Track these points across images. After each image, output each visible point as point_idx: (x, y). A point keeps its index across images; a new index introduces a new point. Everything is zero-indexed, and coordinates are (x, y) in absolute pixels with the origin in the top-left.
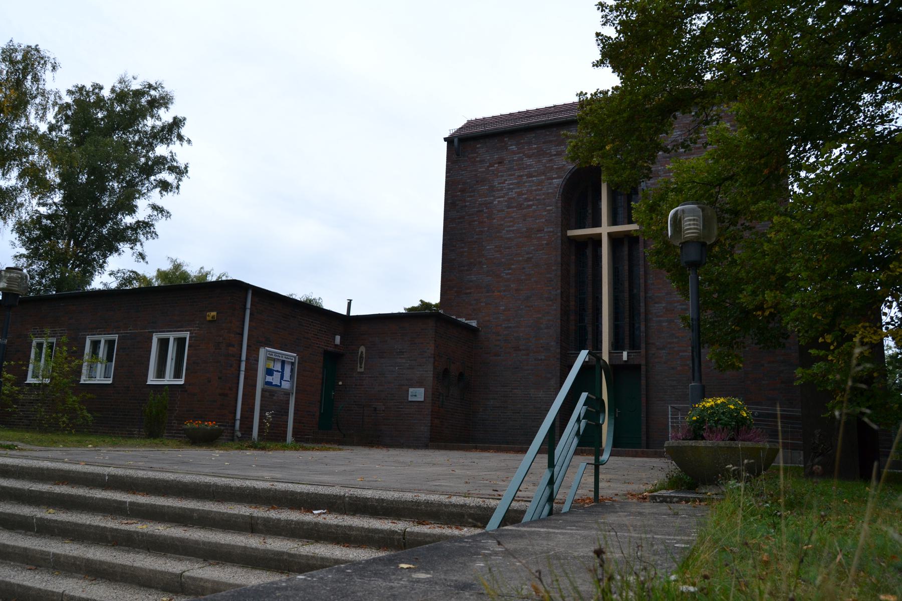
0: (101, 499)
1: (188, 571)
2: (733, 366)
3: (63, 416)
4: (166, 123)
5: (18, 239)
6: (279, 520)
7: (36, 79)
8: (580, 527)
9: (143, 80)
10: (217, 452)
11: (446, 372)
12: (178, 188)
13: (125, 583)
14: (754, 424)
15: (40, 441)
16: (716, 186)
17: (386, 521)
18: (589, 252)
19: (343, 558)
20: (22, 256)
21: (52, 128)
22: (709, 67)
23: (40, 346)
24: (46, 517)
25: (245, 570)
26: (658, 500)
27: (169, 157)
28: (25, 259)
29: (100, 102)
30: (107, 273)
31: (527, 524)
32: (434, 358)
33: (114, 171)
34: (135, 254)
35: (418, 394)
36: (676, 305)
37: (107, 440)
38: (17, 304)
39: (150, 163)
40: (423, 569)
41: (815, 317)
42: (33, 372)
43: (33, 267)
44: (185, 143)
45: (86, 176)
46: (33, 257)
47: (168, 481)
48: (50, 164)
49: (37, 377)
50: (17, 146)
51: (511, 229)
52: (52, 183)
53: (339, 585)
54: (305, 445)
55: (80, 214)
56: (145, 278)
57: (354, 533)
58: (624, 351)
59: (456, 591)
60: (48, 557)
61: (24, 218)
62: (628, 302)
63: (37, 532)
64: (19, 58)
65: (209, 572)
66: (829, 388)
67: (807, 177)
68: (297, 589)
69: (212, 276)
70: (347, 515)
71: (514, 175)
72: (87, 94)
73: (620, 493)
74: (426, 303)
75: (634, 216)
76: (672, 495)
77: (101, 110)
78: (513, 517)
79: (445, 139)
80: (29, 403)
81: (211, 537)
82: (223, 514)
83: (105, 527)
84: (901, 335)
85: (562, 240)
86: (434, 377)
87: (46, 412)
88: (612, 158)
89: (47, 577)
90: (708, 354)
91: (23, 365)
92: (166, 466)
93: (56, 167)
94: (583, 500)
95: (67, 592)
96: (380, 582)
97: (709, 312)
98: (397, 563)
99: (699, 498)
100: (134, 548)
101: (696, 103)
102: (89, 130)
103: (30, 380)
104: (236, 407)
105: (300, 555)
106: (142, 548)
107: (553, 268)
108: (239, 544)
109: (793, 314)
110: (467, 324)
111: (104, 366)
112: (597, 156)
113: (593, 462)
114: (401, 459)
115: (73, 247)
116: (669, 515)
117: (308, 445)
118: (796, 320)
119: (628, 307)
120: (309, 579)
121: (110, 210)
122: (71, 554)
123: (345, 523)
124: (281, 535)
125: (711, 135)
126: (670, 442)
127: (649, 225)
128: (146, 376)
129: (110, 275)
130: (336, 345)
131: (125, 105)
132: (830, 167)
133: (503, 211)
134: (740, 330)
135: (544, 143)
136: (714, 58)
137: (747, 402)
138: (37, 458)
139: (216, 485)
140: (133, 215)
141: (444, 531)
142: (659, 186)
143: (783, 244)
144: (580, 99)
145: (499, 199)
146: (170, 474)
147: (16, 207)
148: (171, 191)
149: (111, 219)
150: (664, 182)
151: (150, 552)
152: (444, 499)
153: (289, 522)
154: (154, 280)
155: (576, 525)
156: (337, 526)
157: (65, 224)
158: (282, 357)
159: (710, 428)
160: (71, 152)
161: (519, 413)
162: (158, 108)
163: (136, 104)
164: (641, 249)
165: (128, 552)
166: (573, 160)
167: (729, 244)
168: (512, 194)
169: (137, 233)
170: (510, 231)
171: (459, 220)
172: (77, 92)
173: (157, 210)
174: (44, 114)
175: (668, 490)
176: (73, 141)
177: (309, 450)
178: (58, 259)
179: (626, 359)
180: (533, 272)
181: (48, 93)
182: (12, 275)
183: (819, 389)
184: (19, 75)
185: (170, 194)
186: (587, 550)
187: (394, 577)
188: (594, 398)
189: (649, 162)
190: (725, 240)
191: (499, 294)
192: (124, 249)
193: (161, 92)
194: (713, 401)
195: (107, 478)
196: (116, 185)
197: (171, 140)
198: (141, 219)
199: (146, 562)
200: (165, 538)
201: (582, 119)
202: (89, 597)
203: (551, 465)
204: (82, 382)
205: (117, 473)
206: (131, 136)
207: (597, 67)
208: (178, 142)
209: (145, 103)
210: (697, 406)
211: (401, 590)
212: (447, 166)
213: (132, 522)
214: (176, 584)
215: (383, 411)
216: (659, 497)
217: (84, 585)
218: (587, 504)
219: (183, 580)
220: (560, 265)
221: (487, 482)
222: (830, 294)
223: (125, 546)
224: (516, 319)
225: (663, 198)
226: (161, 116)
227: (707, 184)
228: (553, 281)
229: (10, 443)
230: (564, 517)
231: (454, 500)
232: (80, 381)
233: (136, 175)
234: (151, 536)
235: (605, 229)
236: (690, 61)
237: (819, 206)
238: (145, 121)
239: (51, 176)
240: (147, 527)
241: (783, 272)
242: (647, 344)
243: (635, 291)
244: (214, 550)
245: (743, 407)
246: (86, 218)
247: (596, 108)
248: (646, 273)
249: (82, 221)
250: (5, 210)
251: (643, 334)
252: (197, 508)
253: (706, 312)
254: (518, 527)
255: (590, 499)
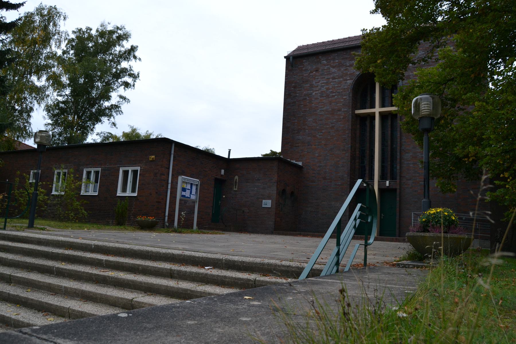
0: (90, 258)
1: (136, 298)
2: (450, 190)
3: (71, 213)
4: (127, 49)
5: (47, 114)
6: (186, 272)
7: (55, 25)
8: (352, 279)
9: (113, 25)
10: (154, 233)
11: (284, 191)
12: (134, 86)
13: (102, 303)
14: (459, 224)
15: (59, 226)
16: (443, 84)
17: (245, 274)
18: (368, 123)
19: (220, 294)
20: (49, 124)
21: (64, 52)
22: (440, 13)
23: (59, 174)
24: (60, 267)
25: (167, 298)
26: (401, 266)
27: (129, 68)
28: (50, 126)
29: (90, 38)
30: (95, 134)
31: (323, 277)
32: (277, 183)
33: (98, 76)
34: (110, 123)
35: (267, 203)
36: (418, 154)
37: (95, 226)
38: (45, 151)
39: (118, 72)
40: (257, 299)
41: (499, 162)
42: (55, 188)
43: (55, 131)
44: (138, 60)
45: (83, 79)
46: (55, 125)
47: (126, 249)
48: (63, 73)
49: (58, 191)
50: (45, 63)
51: (323, 109)
52: (65, 84)
53: (208, 306)
54: (203, 231)
55: (80, 101)
56: (116, 137)
57: (227, 280)
58: (387, 180)
59: (273, 312)
60: (61, 289)
61: (50, 103)
62: (390, 152)
63: (56, 275)
64: (46, 13)
65: (147, 299)
66: (506, 204)
67: (497, 79)
68: (185, 308)
69: (153, 136)
70: (224, 270)
71: (324, 78)
72: (83, 33)
73: (380, 262)
74: (274, 152)
75: (394, 102)
76: (409, 263)
77: (91, 42)
78: (314, 273)
79: (285, 57)
80: (54, 205)
81: (148, 280)
82: (156, 267)
83: (92, 273)
84: (514, 170)
85: (352, 116)
86: (277, 194)
87: (63, 210)
88: (381, 68)
89: (61, 299)
90: (435, 183)
91: (50, 184)
92: (126, 241)
93: (67, 74)
94: (358, 265)
95: (71, 307)
96: (232, 306)
97: (437, 159)
98: (243, 296)
99: (424, 266)
100: (107, 285)
101: (432, 35)
102: (85, 53)
103: (54, 193)
104: (165, 209)
105: (197, 291)
106: (111, 285)
107: (346, 132)
108: (164, 284)
109: (485, 160)
110: (296, 164)
111: (93, 185)
112: (372, 67)
113: (364, 244)
114: (257, 240)
115: (77, 119)
116: (405, 274)
117: (205, 231)
118: (487, 164)
119: (390, 155)
120: (193, 303)
121: (97, 99)
122: (73, 287)
123: (222, 274)
124: (187, 280)
125: (441, 54)
126: (410, 234)
127: (403, 107)
128: (116, 191)
129: (97, 135)
130: (222, 175)
131: (104, 39)
132: (511, 73)
133: (318, 99)
134: (455, 169)
135: (342, 59)
136: (444, 8)
137: (454, 211)
138: (56, 235)
139: (152, 252)
140: (109, 101)
141: (277, 280)
142: (409, 85)
143: (481, 118)
144: (363, 33)
145: (316, 92)
146: (127, 245)
147: (45, 97)
148: (130, 87)
149: (97, 103)
150: (412, 82)
151: (116, 287)
152: (278, 262)
153: (191, 273)
154: (121, 138)
155: (350, 278)
156: (218, 276)
157: (72, 107)
158: (191, 181)
159: (433, 226)
160: (75, 66)
161: (326, 215)
162: (122, 40)
163: (110, 38)
164: (399, 122)
165: (104, 287)
166: (358, 69)
167: (450, 119)
168: (324, 89)
169: (111, 112)
170: (322, 110)
171: (293, 104)
172: (78, 32)
173: (122, 98)
174: (60, 45)
175: (408, 261)
176: (76, 60)
177: (206, 233)
178: (68, 126)
179: (388, 185)
180: (335, 134)
181: (62, 33)
182: (42, 134)
183: (500, 204)
184: (46, 22)
185: (130, 89)
186: (353, 292)
187: (240, 303)
188: (365, 207)
189: (404, 70)
190: (448, 116)
191: (315, 147)
192: (104, 120)
193: (124, 31)
194: (435, 210)
195: (93, 247)
196: (99, 84)
197: (130, 59)
198: (114, 103)
199: (113, 292)
200: (124, 280)
201: (364, 44)
202: (83, 310)
203: (338, 244)
204: (82, 194)
205: (98, 244)
206: (108, 56)
207: (373, 14)
208: (134, 60)
209: (115, 38)
210: (425, 212)
211: (242, 311)
212: (286, 72)
213: (106, 271)
214: (129, 305)
215: (248, 212)
216: (402, 264)
217: (80, 304)
218: (360, 267)
219: (133, 303)
220: (351, 130)
221: (304, 253)
222: (507, 148)
223: (102, 284)
224: (324, 162)
225: (411, 91)
226: (124, 45)
227: (438, 83)
228: (346, 139)
229: (42, 227)
230: (344, 274)
231: (284, 263)
232: (80, 194)
233: (111, 78)
234: (116, 278)
235: (377, 110)
236: (429, 10)
237: (503, 96)
238: (115, 48)
239: (64, 80)
240: (114, 274)
241: (481, 135)
242: (400, 176)
243: (394, 146)
244: (150, 287)
245: (453, 214)
246: (83, 103)
247: (372, 38)
248: (401, 136)
249: (81, 104)
250: (39, 98)
251: (398, 171)
252: (142, 264)
253: (435, 159)
254: (316, 278)
255: (361, 264)
